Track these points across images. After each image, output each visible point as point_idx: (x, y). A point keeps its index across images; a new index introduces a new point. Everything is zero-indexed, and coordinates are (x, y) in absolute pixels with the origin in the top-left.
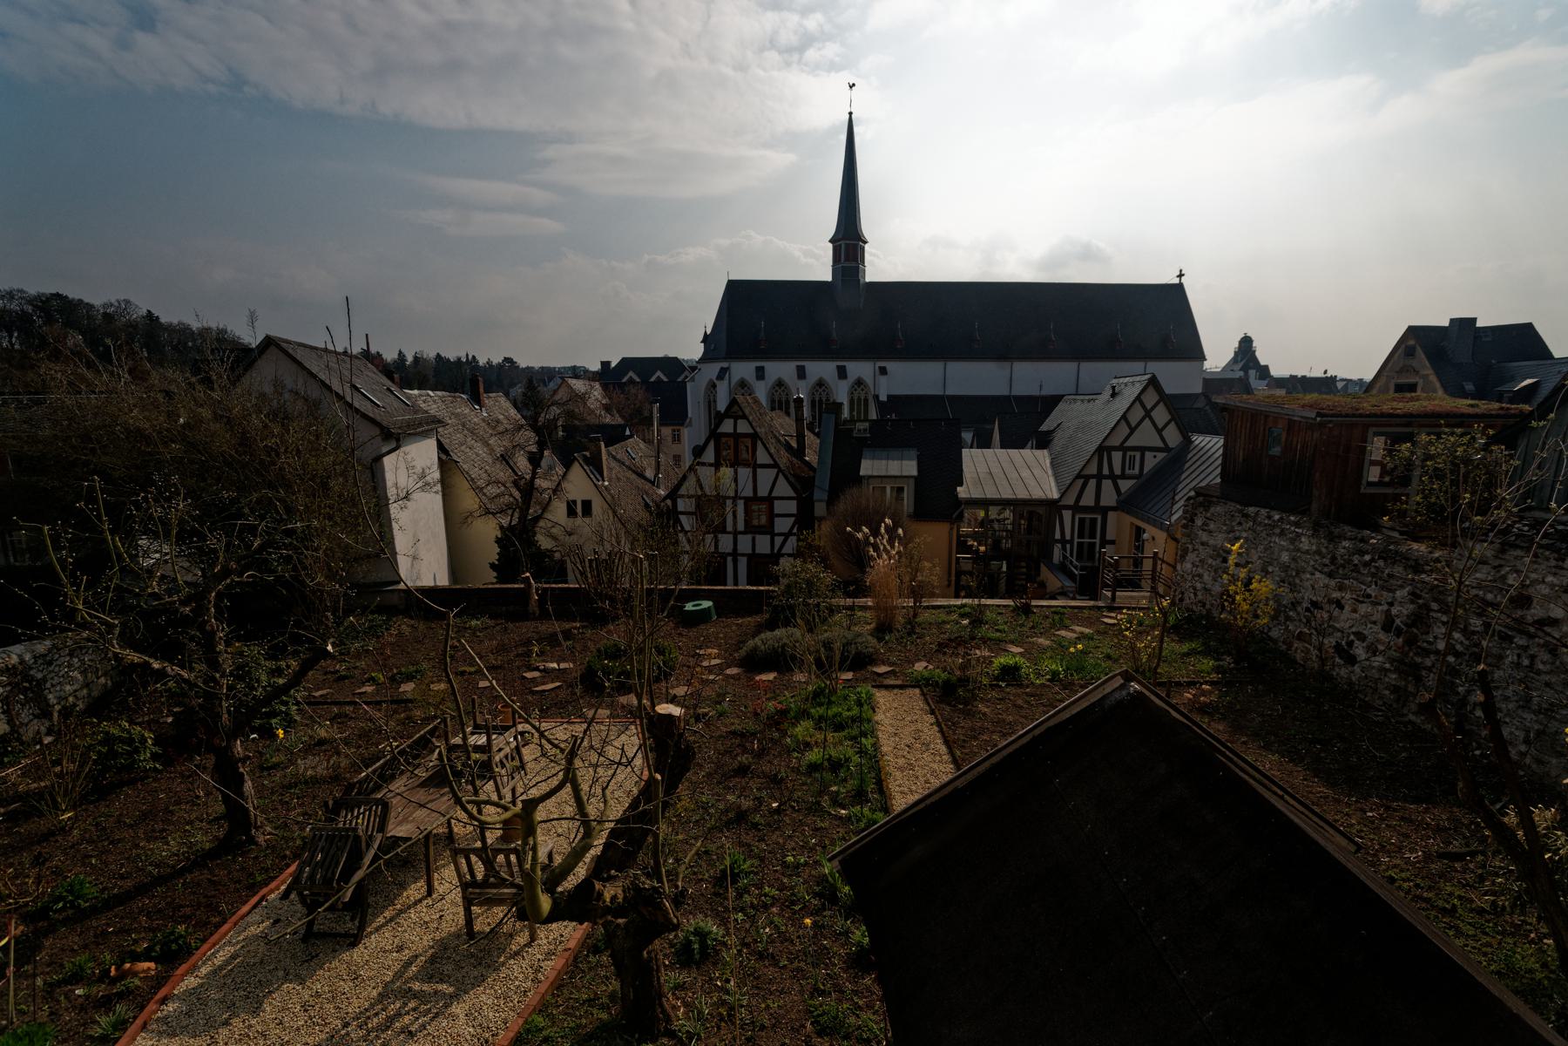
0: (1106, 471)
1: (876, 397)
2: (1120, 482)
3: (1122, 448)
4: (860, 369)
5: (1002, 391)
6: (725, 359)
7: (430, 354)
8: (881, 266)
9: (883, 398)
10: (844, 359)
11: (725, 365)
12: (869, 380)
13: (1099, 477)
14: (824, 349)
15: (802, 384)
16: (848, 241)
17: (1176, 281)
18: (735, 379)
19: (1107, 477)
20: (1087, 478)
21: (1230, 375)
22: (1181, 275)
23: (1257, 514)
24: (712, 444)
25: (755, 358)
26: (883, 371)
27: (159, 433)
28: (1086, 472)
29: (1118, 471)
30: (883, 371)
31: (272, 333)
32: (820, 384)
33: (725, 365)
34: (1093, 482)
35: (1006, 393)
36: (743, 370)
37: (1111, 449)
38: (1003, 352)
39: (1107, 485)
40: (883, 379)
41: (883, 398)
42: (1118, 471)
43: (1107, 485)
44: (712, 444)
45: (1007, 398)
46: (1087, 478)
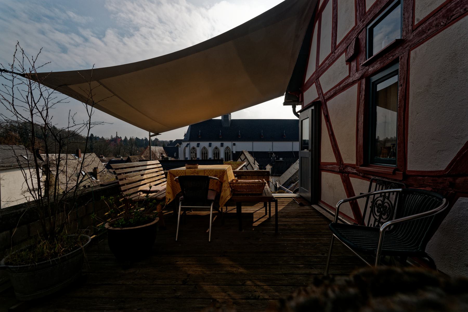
1: (233, 152)
4: (228, 144)
5: (290, 150)
6: (189, 141)
7: (135, 137)
9: (234, 152)
10: (223, 141)
11: (188, 143)
12: (230, 147)
15: (210, 148)
18: (191, 147)
23: (59, 159)
24: (337, 43)
25: (221, 141)
26: (234, 144)
27: (37, 132)
30: (234, 144)
32: (216, 148)
33: (188, 143)
35: (291, 150)
40: (234, 147)
41: (234, 152)
44: (337, 43)
45: (291, 152)
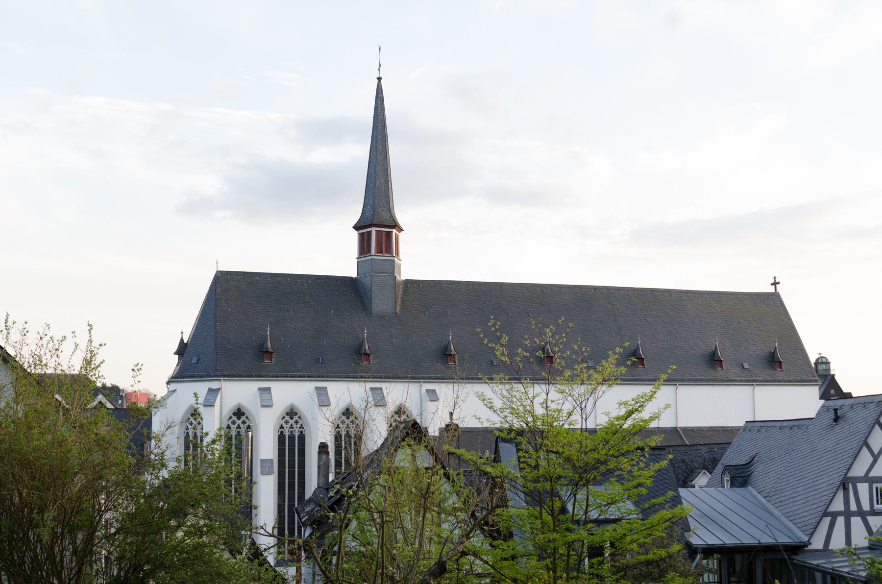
0: (853, 507)
2: (870, 519)
3: (866, 479)
8: (419, 258)
13: (847, 514)
14: (356, 363)
16: (377, 228)
17: (771, 289)
19: (855, 514)
20: (834, 516)
21: (824, 388)
22: (775, 284)
28: (832, 508)
29: (866, 507)
31: (818, 397)
34: (841, 520)
36: (238, 392)
37: (856, 480)
38: (637, 367)
39: (856, 521)
40: (431, 406)
42: (866, 507)
43: (856, 521)
46: (834, 516)
